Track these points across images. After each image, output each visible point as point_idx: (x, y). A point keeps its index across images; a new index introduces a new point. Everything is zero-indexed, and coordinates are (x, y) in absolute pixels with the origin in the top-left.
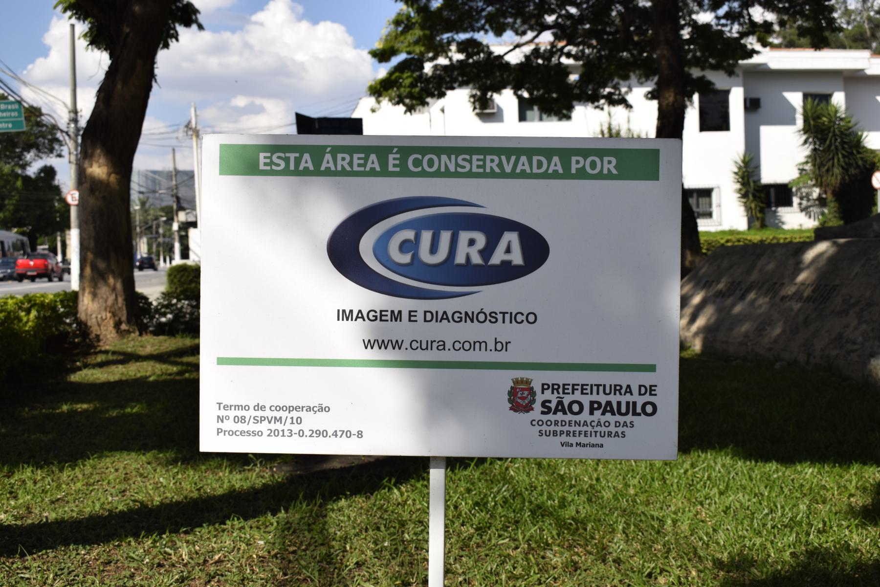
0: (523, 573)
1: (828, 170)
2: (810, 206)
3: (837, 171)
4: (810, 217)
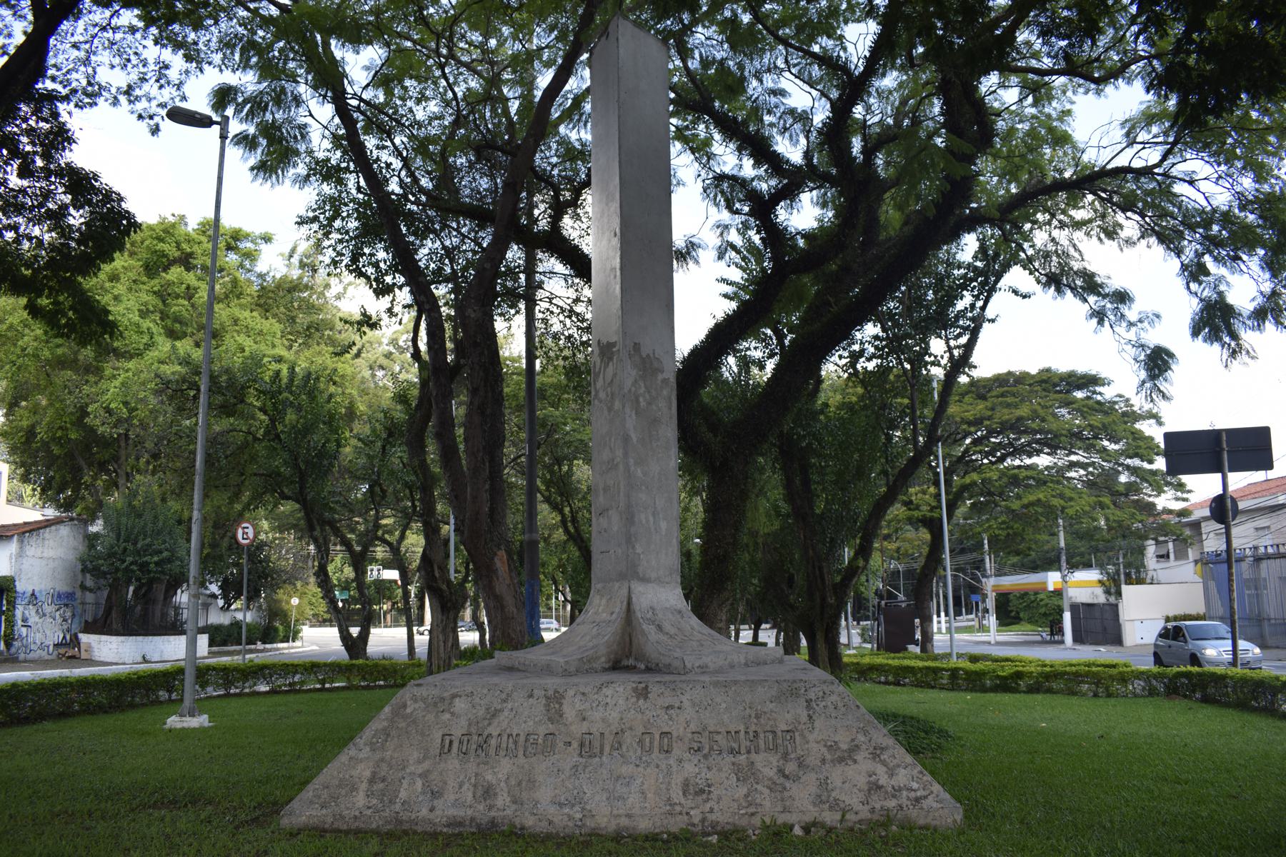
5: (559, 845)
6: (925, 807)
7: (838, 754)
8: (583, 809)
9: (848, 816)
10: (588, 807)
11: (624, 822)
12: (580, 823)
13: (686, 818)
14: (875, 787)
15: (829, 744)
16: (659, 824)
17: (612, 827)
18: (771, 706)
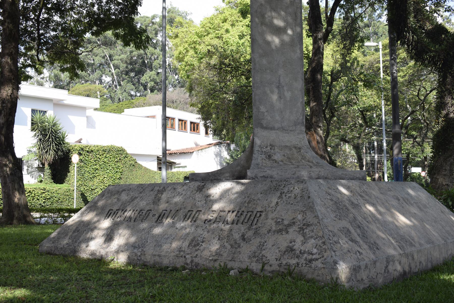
0: (130, 16)
1: (46, 152)
2: (33, 171)
3: (52, 152)
4: (33, 177)
5: (426, 274)
6: (313, 266)
7: (280, 227)
8: (142, 250)
9: (266, 267)
10: (144, 250)
11: (157, 258)
12: (139, 258)
13: (184, 259)
14: (290, 250)
15: (279, 220)
16: (172, 262)
17: (430, 266)
18: (259, 196)
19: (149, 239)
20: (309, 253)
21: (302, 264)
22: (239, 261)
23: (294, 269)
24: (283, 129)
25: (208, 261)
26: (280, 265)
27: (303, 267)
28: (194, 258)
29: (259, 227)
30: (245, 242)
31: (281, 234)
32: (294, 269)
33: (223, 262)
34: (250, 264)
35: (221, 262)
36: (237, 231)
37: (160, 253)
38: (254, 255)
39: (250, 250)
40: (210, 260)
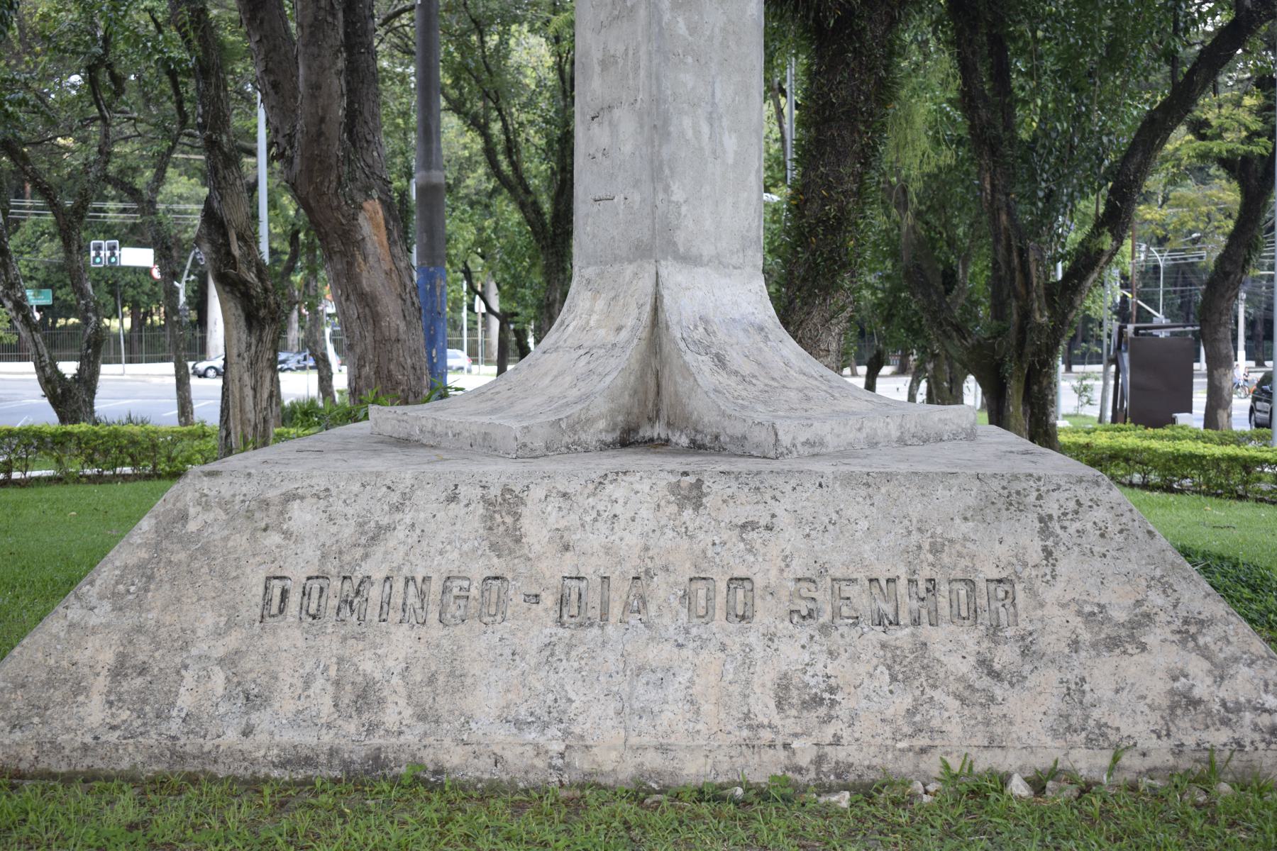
7: (1107, 630)
9: (1125, 760)
11: (653, 760)
13: (782, 754)
19: (568, 688)
20: (1256, 709)
21: (1252, 743)
22: (1019, 746)
23: (1229, 760)
24: (720, 263)
25: (890, 756)
26: (1179, 750)
27: (1260, 752)
28: (828, 749)
29: (1031, 634)
30: (1006, 685)
31: (1125, 652)
32: (1229, 760)
33: (955, 755)
34: (1066, 755)
35: (947, 753)
36: (950, 646)
37: (664, 741)
38: (1064, 727)
39: (1043, 709)
40: (902, 750)
